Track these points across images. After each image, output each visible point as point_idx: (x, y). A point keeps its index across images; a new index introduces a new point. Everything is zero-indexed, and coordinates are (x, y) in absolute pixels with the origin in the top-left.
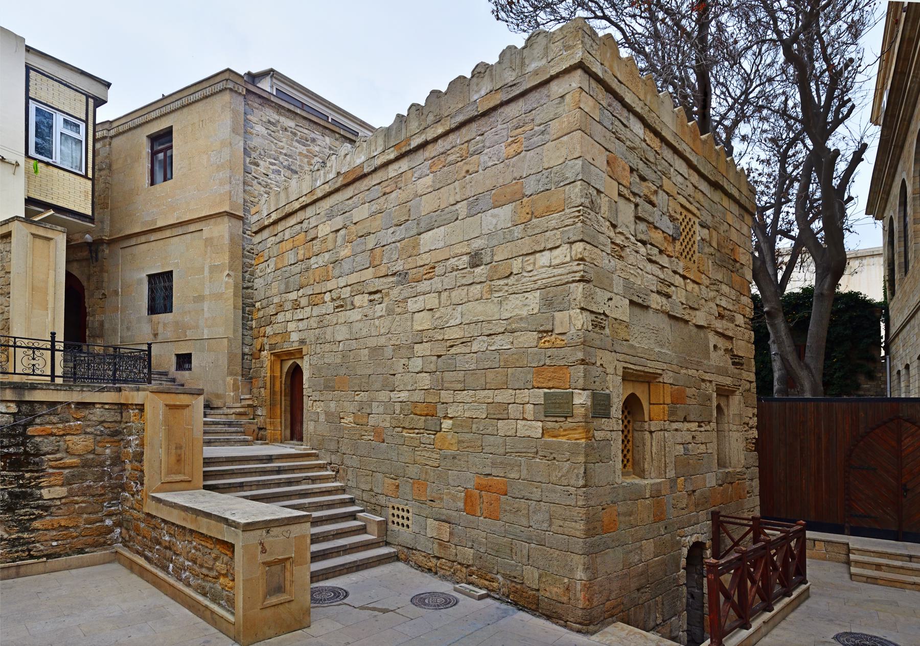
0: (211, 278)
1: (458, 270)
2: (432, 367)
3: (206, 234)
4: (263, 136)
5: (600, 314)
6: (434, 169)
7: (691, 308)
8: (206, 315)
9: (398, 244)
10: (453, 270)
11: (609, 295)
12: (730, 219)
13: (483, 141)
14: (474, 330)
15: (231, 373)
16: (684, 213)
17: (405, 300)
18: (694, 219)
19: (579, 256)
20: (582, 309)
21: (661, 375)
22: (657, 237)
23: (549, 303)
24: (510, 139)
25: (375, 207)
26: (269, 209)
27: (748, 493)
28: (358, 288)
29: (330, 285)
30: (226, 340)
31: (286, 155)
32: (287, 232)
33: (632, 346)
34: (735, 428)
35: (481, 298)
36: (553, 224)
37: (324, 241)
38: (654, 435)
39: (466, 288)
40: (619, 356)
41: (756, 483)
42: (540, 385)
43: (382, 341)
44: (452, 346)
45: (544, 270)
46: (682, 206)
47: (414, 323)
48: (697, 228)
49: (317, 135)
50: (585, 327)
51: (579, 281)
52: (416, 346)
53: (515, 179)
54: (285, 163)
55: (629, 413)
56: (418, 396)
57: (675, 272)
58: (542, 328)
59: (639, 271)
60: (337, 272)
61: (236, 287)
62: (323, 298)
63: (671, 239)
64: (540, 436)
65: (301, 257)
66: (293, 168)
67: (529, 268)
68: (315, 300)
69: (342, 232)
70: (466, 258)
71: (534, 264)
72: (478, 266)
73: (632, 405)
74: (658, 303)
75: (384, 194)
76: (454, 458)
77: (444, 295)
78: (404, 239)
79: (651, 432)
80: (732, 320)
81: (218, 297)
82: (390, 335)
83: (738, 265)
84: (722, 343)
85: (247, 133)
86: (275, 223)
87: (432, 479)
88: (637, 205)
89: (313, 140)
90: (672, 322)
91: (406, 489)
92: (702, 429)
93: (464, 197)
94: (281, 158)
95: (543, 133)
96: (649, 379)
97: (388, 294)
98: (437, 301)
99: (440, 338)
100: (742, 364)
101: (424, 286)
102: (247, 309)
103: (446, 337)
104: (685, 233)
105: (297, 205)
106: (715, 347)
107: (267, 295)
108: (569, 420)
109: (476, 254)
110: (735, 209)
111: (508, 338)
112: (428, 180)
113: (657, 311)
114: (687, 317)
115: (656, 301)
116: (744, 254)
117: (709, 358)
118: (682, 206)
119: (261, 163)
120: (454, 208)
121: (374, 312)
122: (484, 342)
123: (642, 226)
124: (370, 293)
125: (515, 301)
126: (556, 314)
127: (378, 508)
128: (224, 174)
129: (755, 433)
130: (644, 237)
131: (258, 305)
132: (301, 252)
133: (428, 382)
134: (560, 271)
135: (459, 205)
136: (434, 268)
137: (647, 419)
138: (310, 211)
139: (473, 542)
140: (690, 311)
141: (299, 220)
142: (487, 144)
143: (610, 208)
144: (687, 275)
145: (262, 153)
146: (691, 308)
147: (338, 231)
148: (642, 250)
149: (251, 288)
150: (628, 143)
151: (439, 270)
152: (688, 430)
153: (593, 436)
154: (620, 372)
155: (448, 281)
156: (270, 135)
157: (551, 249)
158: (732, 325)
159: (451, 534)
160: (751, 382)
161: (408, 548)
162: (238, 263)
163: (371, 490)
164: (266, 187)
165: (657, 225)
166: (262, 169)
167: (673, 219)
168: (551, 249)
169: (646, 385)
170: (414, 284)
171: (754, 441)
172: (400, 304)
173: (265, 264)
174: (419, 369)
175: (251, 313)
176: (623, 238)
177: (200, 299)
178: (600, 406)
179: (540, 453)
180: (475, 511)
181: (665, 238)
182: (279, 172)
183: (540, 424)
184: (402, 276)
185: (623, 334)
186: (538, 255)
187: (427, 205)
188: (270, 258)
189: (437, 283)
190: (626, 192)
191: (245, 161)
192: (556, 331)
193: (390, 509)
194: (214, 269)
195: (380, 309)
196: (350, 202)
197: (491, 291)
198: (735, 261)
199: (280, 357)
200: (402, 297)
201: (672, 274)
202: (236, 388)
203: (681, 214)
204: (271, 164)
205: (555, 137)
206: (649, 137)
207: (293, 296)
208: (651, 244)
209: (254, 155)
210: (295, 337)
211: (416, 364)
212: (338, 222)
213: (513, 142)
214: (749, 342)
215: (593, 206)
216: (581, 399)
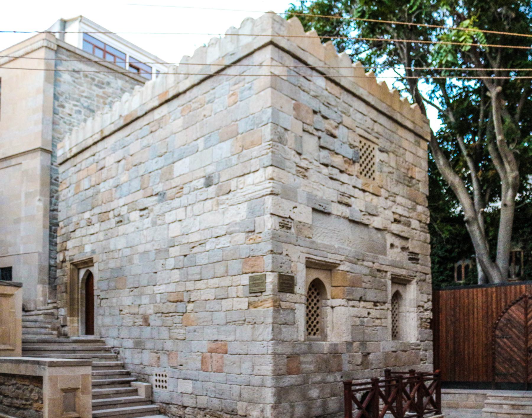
0: (26, 203)
1: (198, 189)
2: (181, 265)
3: (24, 167)
4: (69, 83)
5: (286, 218)
6: (184, 114)
7: (370, 214)
8: (23, 234)
9: (159, 171)
10: (195, 189)
11: (295, 204)
12: (405, 144)
13: (214, 93)
14: (207, 234)
15: (41, 282)
16: (364, 141)
17: (163, 214)
18: (372, 145)
19: (271, 177)
20: (272, 214)
21: (339, 264)
22: (338, 161)
23: (252, 212)
24: (231, 93)
25: (145, 142)
26: (70, 144)
27: (421, 360)
28: (132, 206)
29: (113, 205)
30: (36, 255)
31: (86, 97)
32: (84, 163)
33: (313, 242)
34: (412, 309)
35: (212, 210)
36: (255, 154)
37: (110, 170)
38: (335, 309)
39: (202, 202)
40: (305, 250)
41: (430, 354)
42: (247, 271)
43: (148, 247)
44: (193, 248)
45: (249, 187)
46: (360, 136)
47: (170, 232)
48: (377, 153)
49: (110, 78)
50: (273, 227)
51: (270, 194)
52: (171, 249)
53: (233, 121)
54: (86, 104)
55: (318, 294)
56: (172, 288)
57: (354, 187)
58: (248, 230)
59: (321, 186)
60: (118, 195)
61: (45, 210)
62: (108, 216)
63: (351, 162)
64: (246, 307)
65: (93, 183)
66: (91, 107)
67: (241, 186)
68: (103, 217)
69: (123, 162)
70: (203, 181)
71: (244, 183)
72: (210, 186)
73: (316, 288)
74: (338, 211)
75: (151, 132)
76: (195, 331)
77: (189, 208)
78: (163, 167)
79: (332, 307)
80: (408, 225)
81: (31, 218)
82: (153, 242)
83: (414, 181)
84: (398, 242)
85: (56, 83)
86: (75, 155)
87: (180, 350)
88: (319, 138)
89: (108, 84)
90: (352, 225)
91: (164, 359)
92: (378, 308)
93: (202, 135)
94: (83, 100)
95: (250, 89)
96: (329, 268)
97: (152, 210)
98: (184, 214)
99: (186, 242)
100: (418, 260)
101: (176, 203)
102: (53, 228)
103: (190, 241)
104: (365, 157)
105: (90, 142)
106: (392, 245)
107: (69, 215)
108: (264, 294)
109: (209, 177)
110: (411, 137)
111: (228, 238)
112: (179, 122)
113: (339, 217)
114: (366, 222)
115: (337, 209)
116: (419, 172)
117: (385, 254)
118: (360, 136)
119: (67, 105)
120: (195, 143)
121: (144, 225)
122: (213, 242)
123: (324, 153)
124: (141, 210)
125: (232, 210)
126: (257, 219)
127: (146, 377)
128: (39, 116)
129: (429, 314)
130: (326, 161)
131: (61, 224)
132: (93, 179)
133: (178, 276)
134: (259, 188)
135: (199, 141)
136: (182, 188)
137: (329, 296)
138: (100, 145)
139: (207, 391)
140: (370, 217)
141: (92, 154)
142: (217, 96)
143: (296, 140)
144: (366, 189)
145: (68, 96)
146: (370, 214)
147: (119, 161)
148: (325, 170)
149: (56, 210)
150: (312, 93)
151: (186, 190)
152: (364, 307)
153: (280, 305)
154: (304, 261)
155: (191, 198)
156: (74, 82)
157: (254, 172)
158: (406, 228)
159: (193, 387)
160: (426, 274)
161: (166, 403)
162: (47, 190)
163: (141, 364)
164: (70, 124)
165: (338, 151)
166: (67, 110)
167: (352, 146)
168: (254, 172)
169: (329, 272)
170: (169, 201)
171: (429, 321)
172: (161, 218)
173: (67, 190)
174: (172, 267)
175: (55, 231)
176: (307, 162)
177: (17, 221)
178: (286, 284)
179: (247, 320)
180: (207, 368)
181: (345, 162)
182: (79, 112)
183: (247, 299)
184: (161, 196)
185: (306, 233)
186: (246, 176)
187: (179, 140)
188: (70, 184)
189: (184, 200)
190: (311, 129)
191: (54, 103)
192: (257, 231)
193: (154, 376)
194: (28, 195)
195: (147, 222)
196: (128, 138)
197: (218, 204)
198: (412, 178)
199: (77, 266)
200: (162, 212)
201: (353, 189)
202: (44, 296)
203: (360, 142)
204: (75, 106)
205: (257, 92)
206: (331, 87)
207: (87, 215)
208: (333, 166)
209: (61, 99)
210: (88, 249)
211: (171, 263)
212: (119, 154)
213: (233, 94)
214: (425, 242)
215: (281, 140)
216: (271, 280)
